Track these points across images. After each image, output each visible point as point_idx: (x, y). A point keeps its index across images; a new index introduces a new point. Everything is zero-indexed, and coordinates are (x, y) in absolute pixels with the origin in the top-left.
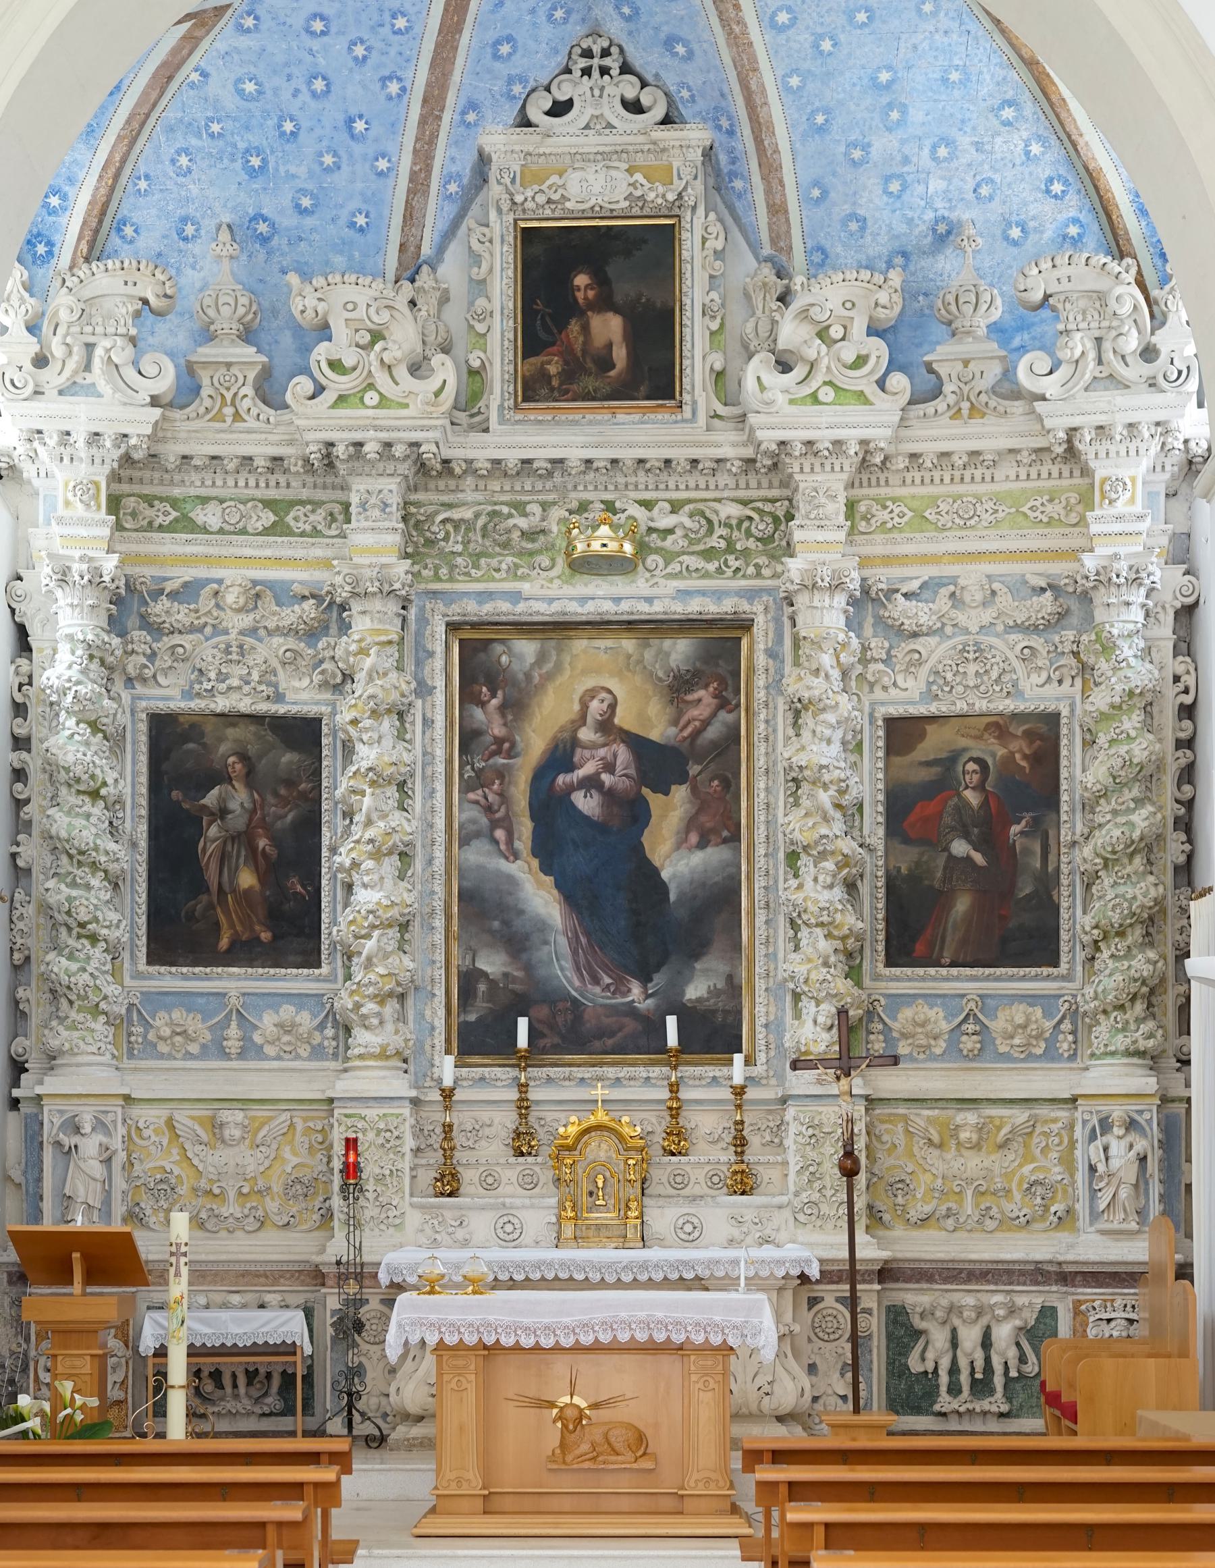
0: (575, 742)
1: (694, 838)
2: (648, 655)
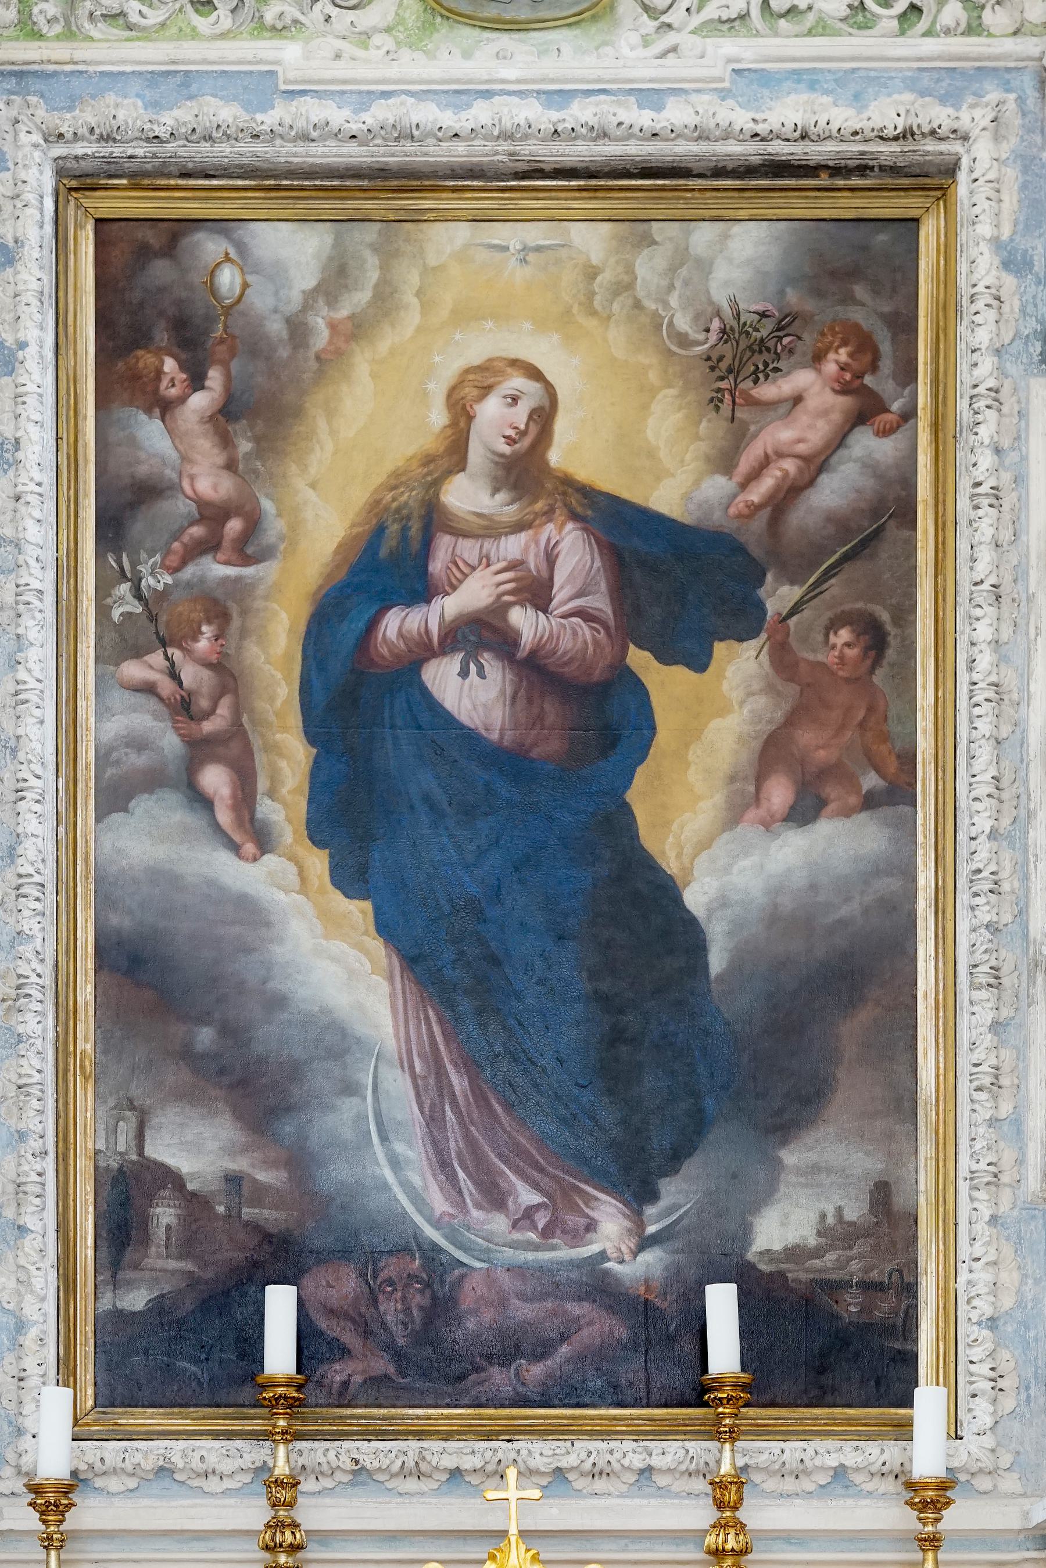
0: (434, 519)
1: (779, 793)
2: (649, 268)
